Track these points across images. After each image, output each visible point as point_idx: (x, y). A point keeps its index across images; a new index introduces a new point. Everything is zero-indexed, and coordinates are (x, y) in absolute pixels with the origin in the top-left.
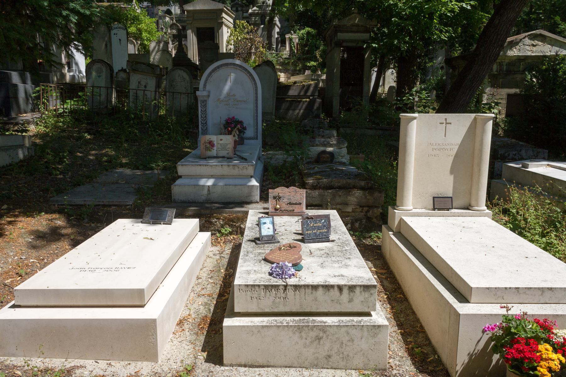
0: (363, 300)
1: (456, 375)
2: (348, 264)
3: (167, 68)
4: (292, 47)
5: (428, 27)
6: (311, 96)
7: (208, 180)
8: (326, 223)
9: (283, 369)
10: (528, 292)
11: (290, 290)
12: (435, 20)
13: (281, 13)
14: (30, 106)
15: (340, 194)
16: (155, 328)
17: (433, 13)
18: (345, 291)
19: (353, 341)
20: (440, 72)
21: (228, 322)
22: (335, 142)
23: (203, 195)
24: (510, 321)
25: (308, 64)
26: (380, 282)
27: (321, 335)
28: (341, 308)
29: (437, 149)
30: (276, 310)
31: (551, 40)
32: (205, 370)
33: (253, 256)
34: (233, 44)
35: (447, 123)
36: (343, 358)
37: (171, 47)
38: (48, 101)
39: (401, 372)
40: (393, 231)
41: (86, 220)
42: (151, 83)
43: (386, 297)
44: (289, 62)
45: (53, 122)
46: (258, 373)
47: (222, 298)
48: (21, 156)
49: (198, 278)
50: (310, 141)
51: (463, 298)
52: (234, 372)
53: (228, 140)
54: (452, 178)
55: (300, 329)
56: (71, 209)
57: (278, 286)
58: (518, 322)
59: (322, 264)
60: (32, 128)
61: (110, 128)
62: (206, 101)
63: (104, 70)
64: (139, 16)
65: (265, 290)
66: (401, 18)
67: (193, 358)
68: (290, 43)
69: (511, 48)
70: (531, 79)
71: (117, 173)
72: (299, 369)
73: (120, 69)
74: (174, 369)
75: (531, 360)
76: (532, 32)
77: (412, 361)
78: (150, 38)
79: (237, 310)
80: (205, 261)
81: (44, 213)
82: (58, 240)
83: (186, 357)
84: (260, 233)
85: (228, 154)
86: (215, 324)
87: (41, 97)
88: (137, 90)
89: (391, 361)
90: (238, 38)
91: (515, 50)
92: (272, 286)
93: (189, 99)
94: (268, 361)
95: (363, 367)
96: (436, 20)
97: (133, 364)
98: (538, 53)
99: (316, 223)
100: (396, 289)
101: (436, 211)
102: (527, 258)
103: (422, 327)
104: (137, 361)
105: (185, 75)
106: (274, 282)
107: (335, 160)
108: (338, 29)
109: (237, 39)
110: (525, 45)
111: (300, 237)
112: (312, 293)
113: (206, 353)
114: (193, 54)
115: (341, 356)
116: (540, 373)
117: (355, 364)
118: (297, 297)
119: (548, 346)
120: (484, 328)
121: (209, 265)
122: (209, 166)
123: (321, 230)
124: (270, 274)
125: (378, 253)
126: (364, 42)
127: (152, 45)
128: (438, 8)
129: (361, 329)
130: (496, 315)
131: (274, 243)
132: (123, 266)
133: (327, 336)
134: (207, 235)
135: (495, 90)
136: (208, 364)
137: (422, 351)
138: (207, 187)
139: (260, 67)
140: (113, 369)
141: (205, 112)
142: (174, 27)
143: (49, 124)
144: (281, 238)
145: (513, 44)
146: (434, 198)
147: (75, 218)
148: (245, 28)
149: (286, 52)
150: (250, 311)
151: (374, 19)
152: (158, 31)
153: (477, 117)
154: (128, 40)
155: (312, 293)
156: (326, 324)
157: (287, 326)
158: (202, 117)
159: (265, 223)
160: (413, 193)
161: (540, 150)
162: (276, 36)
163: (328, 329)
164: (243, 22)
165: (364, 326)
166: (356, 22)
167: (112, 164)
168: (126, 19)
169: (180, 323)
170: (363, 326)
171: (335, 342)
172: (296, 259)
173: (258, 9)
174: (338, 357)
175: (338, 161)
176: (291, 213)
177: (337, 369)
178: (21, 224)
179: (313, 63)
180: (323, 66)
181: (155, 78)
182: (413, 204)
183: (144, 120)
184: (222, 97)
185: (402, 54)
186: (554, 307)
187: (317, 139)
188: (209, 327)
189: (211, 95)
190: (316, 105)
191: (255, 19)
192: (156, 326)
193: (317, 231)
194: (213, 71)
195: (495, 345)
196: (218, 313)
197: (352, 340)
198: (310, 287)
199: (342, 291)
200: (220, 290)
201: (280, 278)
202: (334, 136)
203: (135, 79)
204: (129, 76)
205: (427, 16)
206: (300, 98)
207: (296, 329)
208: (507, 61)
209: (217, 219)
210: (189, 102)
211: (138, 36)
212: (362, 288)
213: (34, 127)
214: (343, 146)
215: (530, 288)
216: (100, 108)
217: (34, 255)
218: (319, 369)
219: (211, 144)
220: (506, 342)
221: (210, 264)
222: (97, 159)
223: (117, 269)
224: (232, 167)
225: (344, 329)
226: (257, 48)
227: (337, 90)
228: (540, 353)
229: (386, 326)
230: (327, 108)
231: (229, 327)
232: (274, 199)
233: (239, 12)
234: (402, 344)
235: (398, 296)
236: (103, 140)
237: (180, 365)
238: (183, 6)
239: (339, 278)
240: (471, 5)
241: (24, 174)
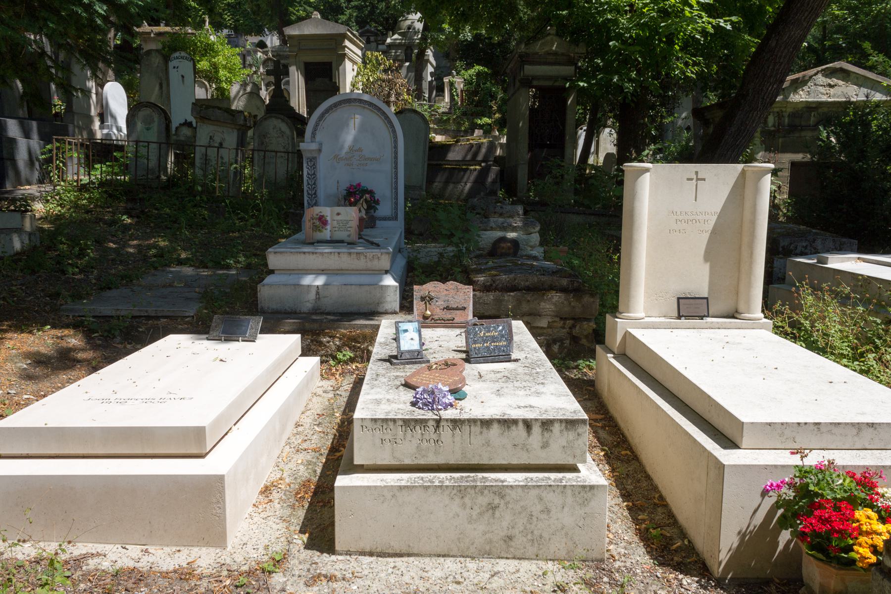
0: (565, 444)
1: (719, 567)
2: (542, 391)
3: (255, 116)
4: (454, 95)
5: (667, 56)
6: (483, 161)
7: (316, 277)
8: (506, 331)
9: (434, 559)
10: (835, 430)
11: (446, 428)
12: (676, 46)
13: (436, 43)
14: (36, 175)
15: (529, 298)
16: (222, 492)
17: (674, 34)
18: (536, 429)
19: (549, 511)
20: (685, 134)
21: (341, 481)
22: (520, 224)
23: (308, 301)
24: (806, 474)
25: (479, 122)
26: (594, 433)
27: (497, 501)
28: (529, 458)
29: (683, 221)
30: (422, 461)
31: (857, 78)
32: (305, 561)
33: (386, 380)
34: (361, 87)
35: (698, 179)
36: (533, 540)
38: (65, 164)
39: (628, 564)
40: (613, 353)
41: (118, 339)
42: (230, 138)
43: (602, 454)
44: (449, 119)
45: (72, 198)
46: (392, 565)
47: (336, 454)
48: (17, 245)
49: (298, 425)
50: (481, 222)
51: (729, 443)
52: (352, 564)
53: (351, 214)
54: (707, 267)
55: (461, 491)
56: (93, 322)
57: (426, 421)
58: (820, 476)
59: (498, 390)
60: (39, 208)
61: (163, 208)
62: (315, 158)
63: (156, 119)
64: (214, 44)
65: (404, 427)
66: (624, 42)
67: (286, 543)
68: (451, 90)
69: (795, 91)
70: (828, 137)
71: (171, 272)
72: (460, 559)
74: (252, 559)
75: (843, 534)
76: (828, 66)
77: (646, 548)
78: (230, 78)
79: (357, 461)
80: (310, 400)
81: (49, 327)
82: (70, 368)
83: (273, 540)
84: (398, 347)
85: (349, 236)
86: (323, 492)
87: (55, 158)
89: (611, 547)
90: (369, 78)
92: (416, 421)
93: (290, 165)
94: (409, 546)
95: (566, 556)
96: (679, 46)
97: (185, 551)
98: (838, 98)
99: (489, 331)
100: (619, 443)
101: (683, 320)
102: (831, 382)
103: (661, 498)
104: (193, 546)
106: (419, 414)
108: (525, 59)
109: (368, 80)
110: (817, 85)
111: (464, 356)
112: (481, 433)
113: (307, 535)
114: (298, 100)
115: (529, 537)
116: (859, 556)
117: (552, 551)
118: (458, 439)
119: (870, 512)
120: (764, 486)
121: (316, 407)
122: (318, 255)
123: (496, 342)
124: (414, 404)
125: (590, 390)
126: (566, 79)
127: (234, 89)
128: (682, 27)
129: (562, 492)
130: (783, 466)
131: (420, 363)
132: (172, 396)
133: (507, 503)
135: (772, 155)
136: (309, 552)
137: (662, 534)
138: (316, 289)
139: (403, 115)
140: (151, 559)
141: (313, 176)
143: (65, 200)
144: (432, 356)
145: (797, 85)
146: (679, 299)
147: (100, 336)
148: (380, 64)
149: (444, 104)
150: (379, 463)
151: (581, 44)
152: (244, 67)
153: (746, 169)
154: (195, 82)
155: (481, 433)
156: (504, 484)
157: (441, 486)
158: (308, 184)
159: (406, 331)
160: (646, 292)
161: (844, 240)
162: (429, 79)
163: (508, 491)
164: (376, 54)
165: (567, 487)
166: (554, 48)
167: (164, 258)
168: (194, 49)
169: (266, 491)
170: (565, 486)
171: (520, 513)
172: (456, 382)
173: (400, 37)
174: (525, 540)
176: (449, 324)
177: (524, 559)
178: (12, 342)
179: (486, 120)
180: (501, 124)
181: (235, 131)
182: (646, 310)
183: (218, 194)
184: (343, 153)
185: (625, 98)
186: (878, 455)
187: (492, 219)
188: (312, 497)
189: (324, 149)
190: (491, 177)
191: (396, 53)
192: (223, 487)
193: (490, 344)
194: (327, 111)
195: (783, 516)
196: (328, 476)
197: (547, 511)
198: (479, 423)
199: (531, 429)
200: (333, 442)
201: (429, 409)
202: (518, 215)
203: (204, 133)
205: (664, 39)
206: (465, 165)
207: (455, 492)
208: (789, 110)
209: (330, 337)
210: (289, 169)
211: (211, 76)
212: (564, 425)
213: (41, 205)
214: (533, 230)
215: (839, 424)
216: (148, 178)
217: (29, 389)
218: (493, 560)
219: (323, 221)
220: (801, 507)
221: (318, 405)
222: (140, 252)
223: (162, 400)
224: (355, 255)
225: (534, 492)
226: (398, 95)
227: (524, 154)
228: (858, 524)
229: (603, 486)
230: (508, 181)
231: (344, 488)
232: (422, 301)
233: (372, 43)
234: (630, 524)
235: (623, 452)
236: (152, 225)
237: (263, 552)
238: (284, 29)
239: (526, 409)
240: (732, 23)
241: (22, 270)
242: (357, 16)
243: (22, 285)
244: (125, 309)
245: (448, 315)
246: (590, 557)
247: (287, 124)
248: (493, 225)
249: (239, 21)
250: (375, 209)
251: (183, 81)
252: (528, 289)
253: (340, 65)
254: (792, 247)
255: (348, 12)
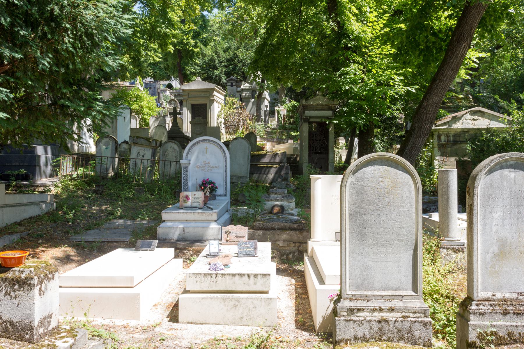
0: (262, 283)
11: (219, 277)
16: (139, 299)
30: (211, 289)
31: (489, 115)
34: (223, 117)
37: (169, 120)
41: (95, 251)
42: (148, 153)
44: (276, 132)
50: (266, 197)
53: (200, 195)
55: (224, 299)
62: (187, 167)
63: (111, 144)
68: (278, 115)
69: (455, 123)
73: (123, 141)
85: (199, 205)
88: (136, 159)
91: (458, 123)
92: (209, 274)
99: (246, 244)
105: (176, 147)
107: (285, 212)
114: (187, 129)
115: (249, 317)
126: (328, 118)
133: (241, 304)
134: (180, 261)
139: (237, 140)
142: (173, 102)
146: (336, 232)
149: (273, 123)
154: (131, 115)
159: (213, 244)
163: (241, 300)
169: (155, 305)
170: (261, 298)
171: (245, 308)
175: (287, 212)
187: (271, 196)
194: (193, 145)
203: (135, 150)
204: (131, 147)
208: (453, 133)
211: (139, 112)
212: (262, 276)
214: (291, 201)
219: (187, 198)
225: (250, 300)
236: (108, 198)
240: (415, 89)
242: (225, 71)
243: (51, 228)
244: (98, 238)
245: (237, 240)
246: (271, 325)
247: (177, 145)
248: (271, 198)
249: (156, 73)
250: (216, 191)
251: (125, 120)
252: (279, 229)
253: (211, 105)
254: (428, 209)
255: (220, 69)
